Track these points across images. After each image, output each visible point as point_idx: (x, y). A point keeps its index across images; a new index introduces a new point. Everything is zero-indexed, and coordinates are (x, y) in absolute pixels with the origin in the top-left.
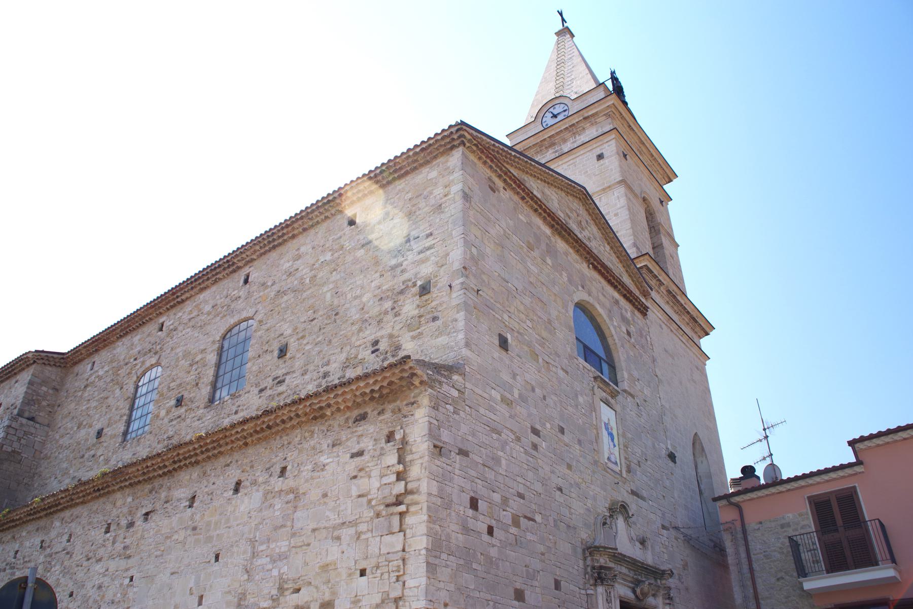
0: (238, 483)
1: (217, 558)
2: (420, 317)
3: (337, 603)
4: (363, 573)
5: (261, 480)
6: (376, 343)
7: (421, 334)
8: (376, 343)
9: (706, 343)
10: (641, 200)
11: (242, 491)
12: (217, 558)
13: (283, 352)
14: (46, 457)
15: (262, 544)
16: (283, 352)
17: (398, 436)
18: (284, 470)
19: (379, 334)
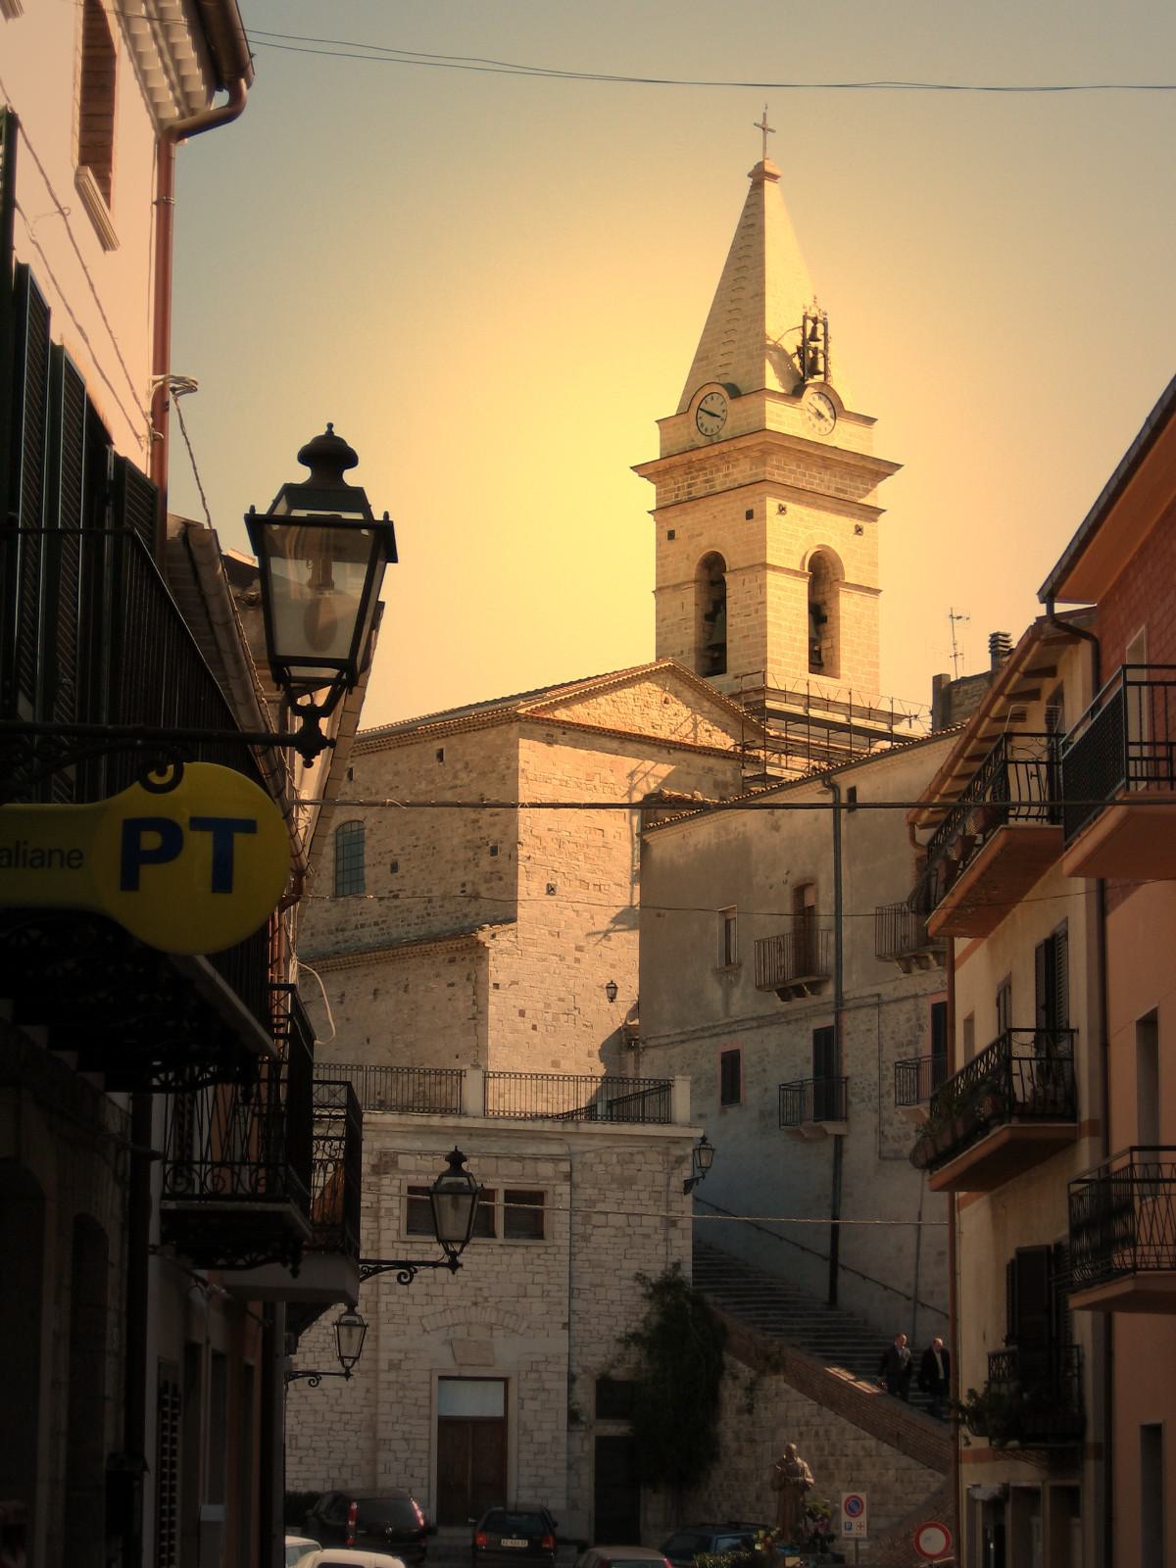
0: (376, 990)
1: (368, 1041)
2: (492, 873)
3: (76, 162)
4: (457, 1057)
5: (392, 991)
6: (464, 885)
7: (492, 888)
8: (464, 885)
9: (800, 345)
10: (688, 569)
11: (380, 998)
12: (368, 1041)
13: (394, 868)
14: (985, 1382)
15: (398, 1035)
16: (394, 868)
17: (473, 977)
18: (407, 986)
19: (466, 878)
